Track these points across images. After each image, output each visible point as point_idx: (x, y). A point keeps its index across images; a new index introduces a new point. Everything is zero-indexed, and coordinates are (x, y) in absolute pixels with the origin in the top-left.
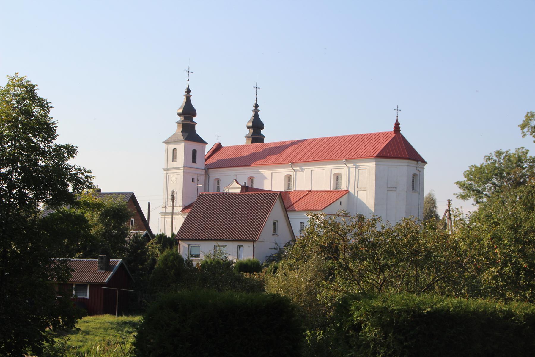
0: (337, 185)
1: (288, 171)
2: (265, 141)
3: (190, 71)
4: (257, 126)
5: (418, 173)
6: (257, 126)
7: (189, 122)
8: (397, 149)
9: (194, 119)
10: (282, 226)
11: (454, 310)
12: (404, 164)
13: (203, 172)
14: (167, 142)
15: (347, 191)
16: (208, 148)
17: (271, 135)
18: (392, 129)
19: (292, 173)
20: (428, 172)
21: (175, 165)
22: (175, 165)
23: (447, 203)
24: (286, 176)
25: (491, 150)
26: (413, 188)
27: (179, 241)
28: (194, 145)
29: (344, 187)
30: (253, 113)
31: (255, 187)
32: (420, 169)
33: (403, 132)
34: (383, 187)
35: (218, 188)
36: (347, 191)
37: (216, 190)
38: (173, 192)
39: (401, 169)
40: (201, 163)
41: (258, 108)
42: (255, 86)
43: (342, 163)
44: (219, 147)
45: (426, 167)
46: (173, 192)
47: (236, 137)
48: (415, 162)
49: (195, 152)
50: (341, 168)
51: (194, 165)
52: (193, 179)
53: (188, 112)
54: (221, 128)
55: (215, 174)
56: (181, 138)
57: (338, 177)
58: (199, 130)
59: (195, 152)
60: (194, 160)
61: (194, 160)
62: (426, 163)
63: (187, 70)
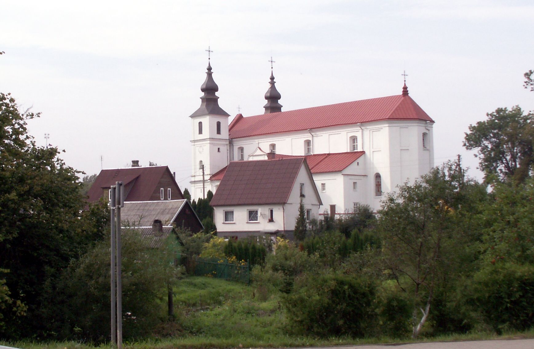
0: (354, 147)
1: (307, 136)
2: (283, 110)
3: (210, 50)
5: (427, 132)
9: (217, 94)
10: (308, 191)
11: (467, 182)
12: (415, 124)
13: (228, 143)
14: (193, 116)
15: (363, 153)
16: (231, 120)
17: (287, 104)
18: (400, 93)
19: (310, 139)
20: (437, 131)
23: (457, 158)
25: (492, 110)
26: (424, 146)
27: (214, 208)
28: (216, 119)
29: (360, 149)
30: (269, 86)
32: (429, 128)
33: (411, 94)
34: (398, 152)
35: (242, 156)
38: (201, 162)
39: (413, 131)
40: (225, 133)
41: (274, 80)
43: (357, 126)
44: (240, 118)
46: (201, 162)
47: (256, 107)
48: (424, 122)
49: (219, 124)
50: (356, 131)
51: (219, 136)
52: (219, 149)
54: (242, 99)
55: (238, 144)
56: (207, 112)
57: (354, 139)
58: (222, 104)
59: (219, 124)
60: (219, 132)
61: (219, 132)
63: (208, 49)
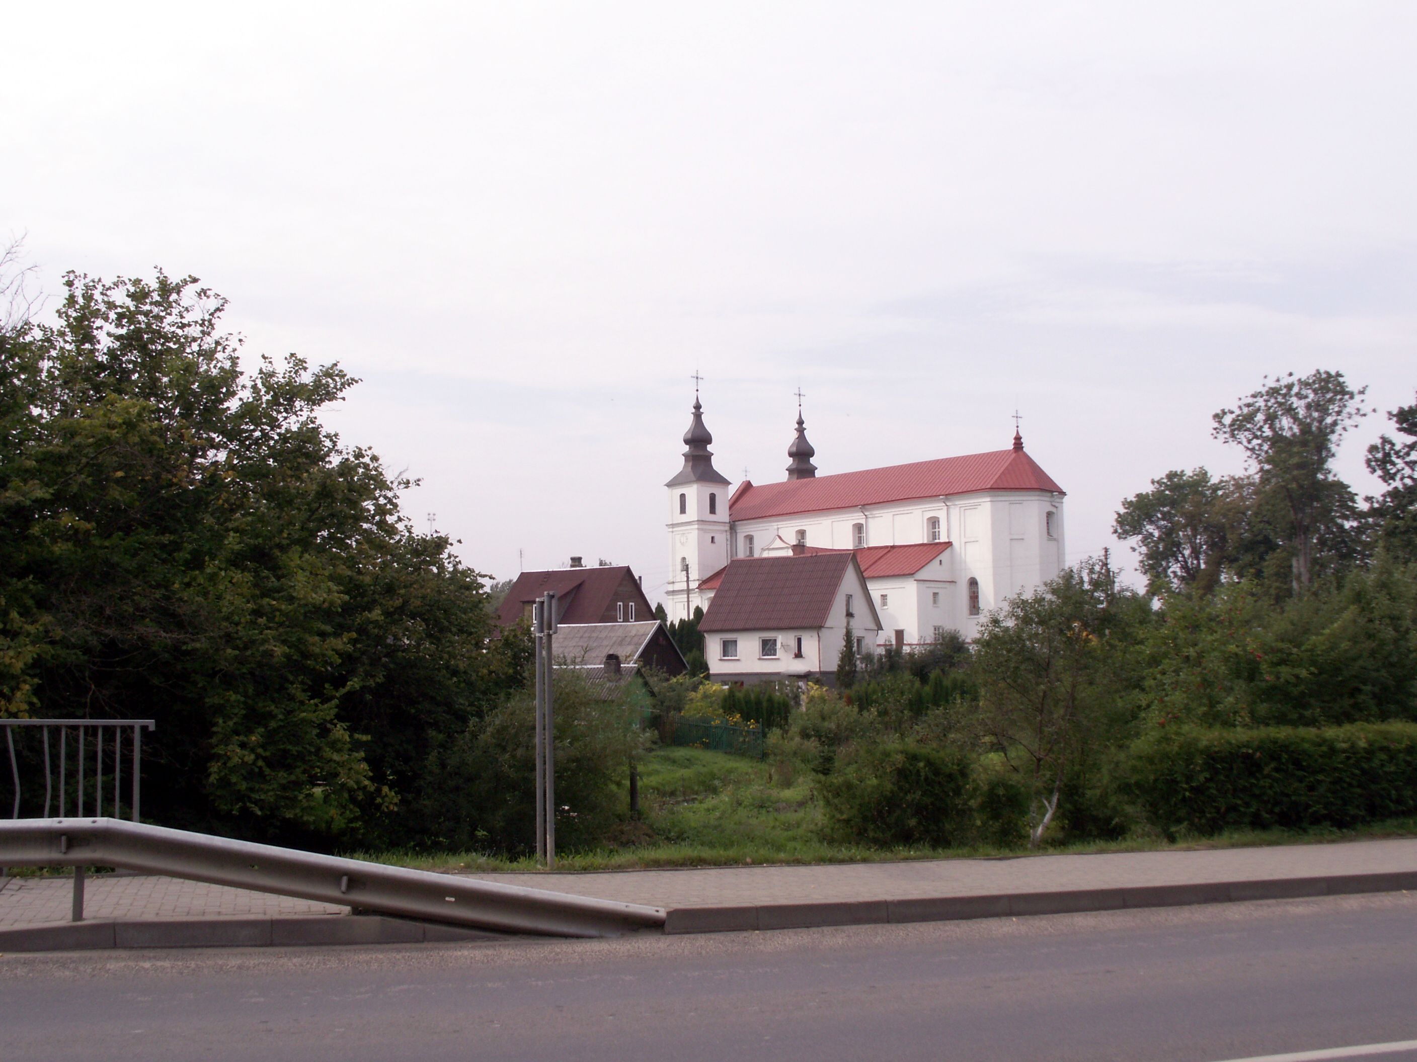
0: (934, 535)
1: (857, 517)
2: (818, 474)
3: (699, 376)
4: (802, 454)
5: (1054, 510)
6: (802, 454)
7: (701, 453)
8: (1016, 476)
10: (859, 606)
12: (1033, 498)
13: (727, 528)
14: (670, 485)
16: (732, 490)
17: (825, 465)
18: (1009, 445)
19: (863, 521)
20: (1069, 507)
21: (684, 518)
22: (684, 518)
24: (854, 525)
26: (1048, 533)
29: (943, 539)
30: (795, 435)
31: (872, 544)
32: (1057, 505)
33: (1029, 448)
36: (949, 544)
37: (748, 553)
38: (684, 559)
40: (723, 513)
41: (804, 426)
42: (797, 392)
44: (747, 487)
45: (1066, 499)
46: (684, 559)
47: (773, 470)
48: (1049, 494)
49: (713, 498)
50: (937, 509)
51: (712, 518)
52: (713, 538)
53: (699, 441)
54: (751, 457)
55: (744, 530)
57: (934, 522)
58: (717, 464)
59: (713, 498)
60: (713, 510)
61: (713, 510)
62: (1064, 494)
63: (695, 375)
